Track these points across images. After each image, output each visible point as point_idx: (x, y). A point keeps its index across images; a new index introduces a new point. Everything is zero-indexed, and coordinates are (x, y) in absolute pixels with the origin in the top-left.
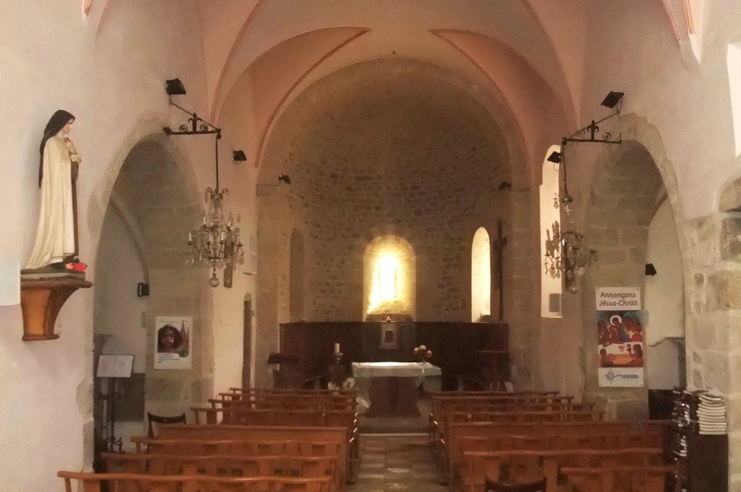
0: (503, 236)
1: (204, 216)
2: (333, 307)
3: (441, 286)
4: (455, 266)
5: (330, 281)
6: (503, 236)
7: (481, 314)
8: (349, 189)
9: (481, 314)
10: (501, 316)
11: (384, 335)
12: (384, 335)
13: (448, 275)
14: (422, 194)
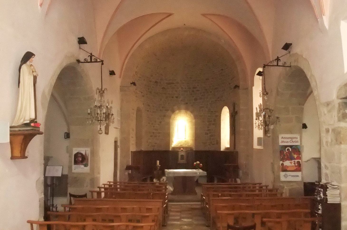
0: (236, 111)
1: (96, 101)
2: (156, 143)
3: (207, 134)
4: (213, 124)
5: (155, 131)
6: (236, 111)
7: (225, 147)
9: (225, 147)
10: (235, 148)
11: (180, 157)
12: (180, 157)
13: (210, 128)
14: (198, 91)
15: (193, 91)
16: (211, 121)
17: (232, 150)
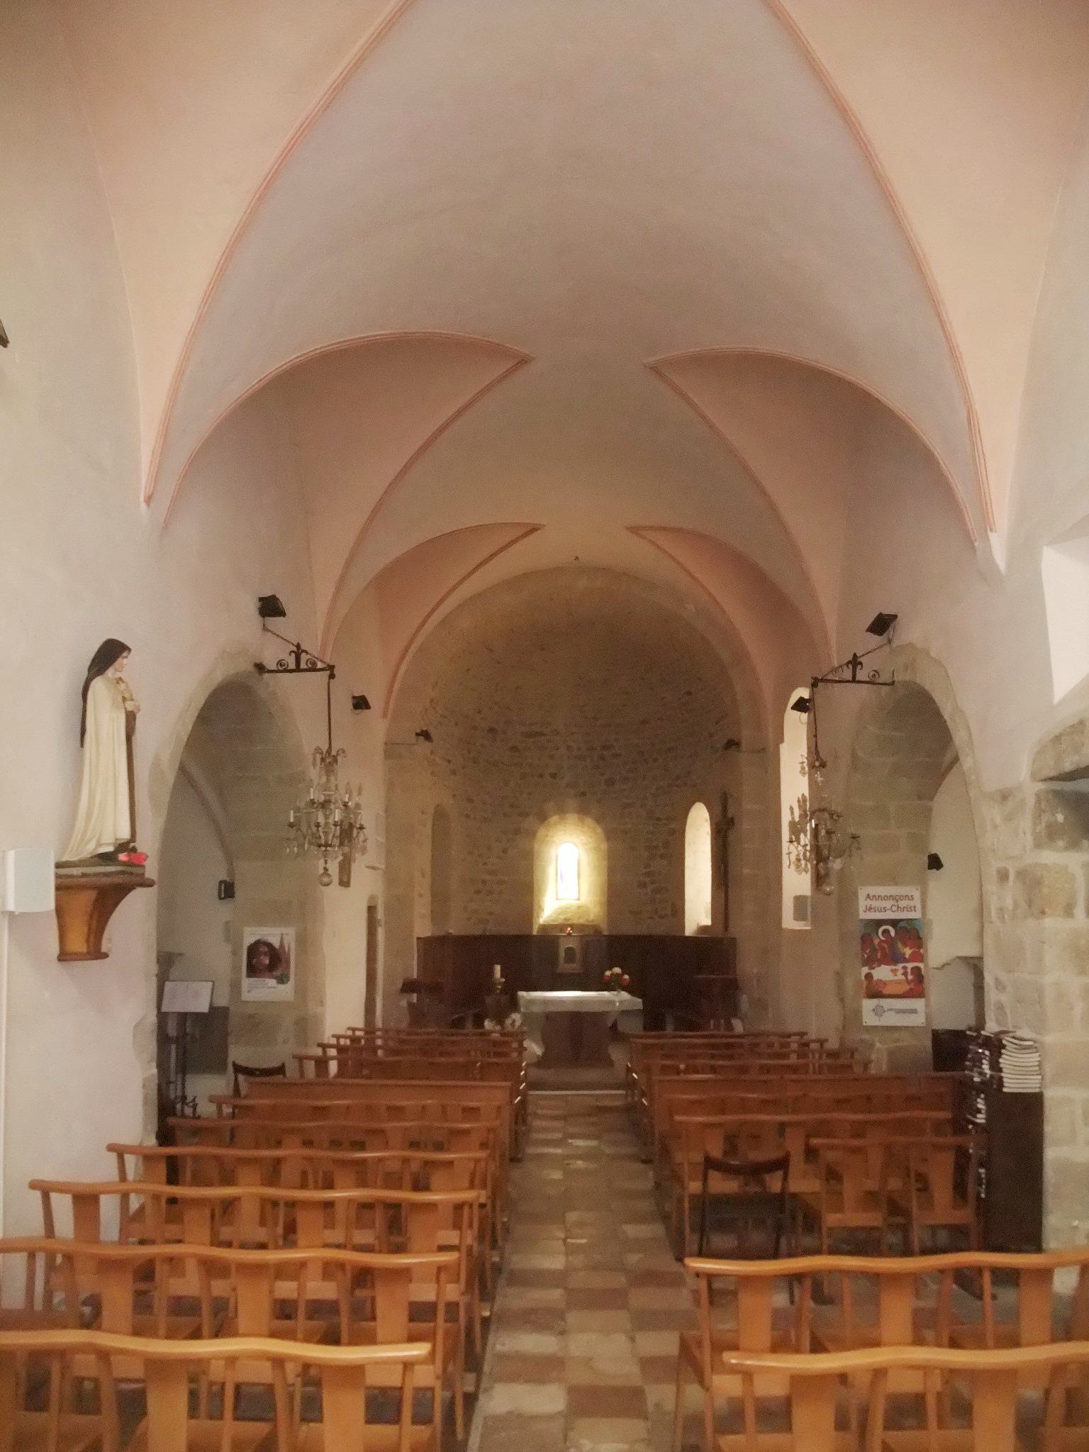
3: (643, 885)
4: (662, 856)
5: (487, 877)
7: (698, 924)
8: (514, 749)
9: (698, 924)
10: (726, 927)
11: (562, 954)
12: (562, 954)
15: (602, 758)
16: (656, 847)
17: (719, 933)
